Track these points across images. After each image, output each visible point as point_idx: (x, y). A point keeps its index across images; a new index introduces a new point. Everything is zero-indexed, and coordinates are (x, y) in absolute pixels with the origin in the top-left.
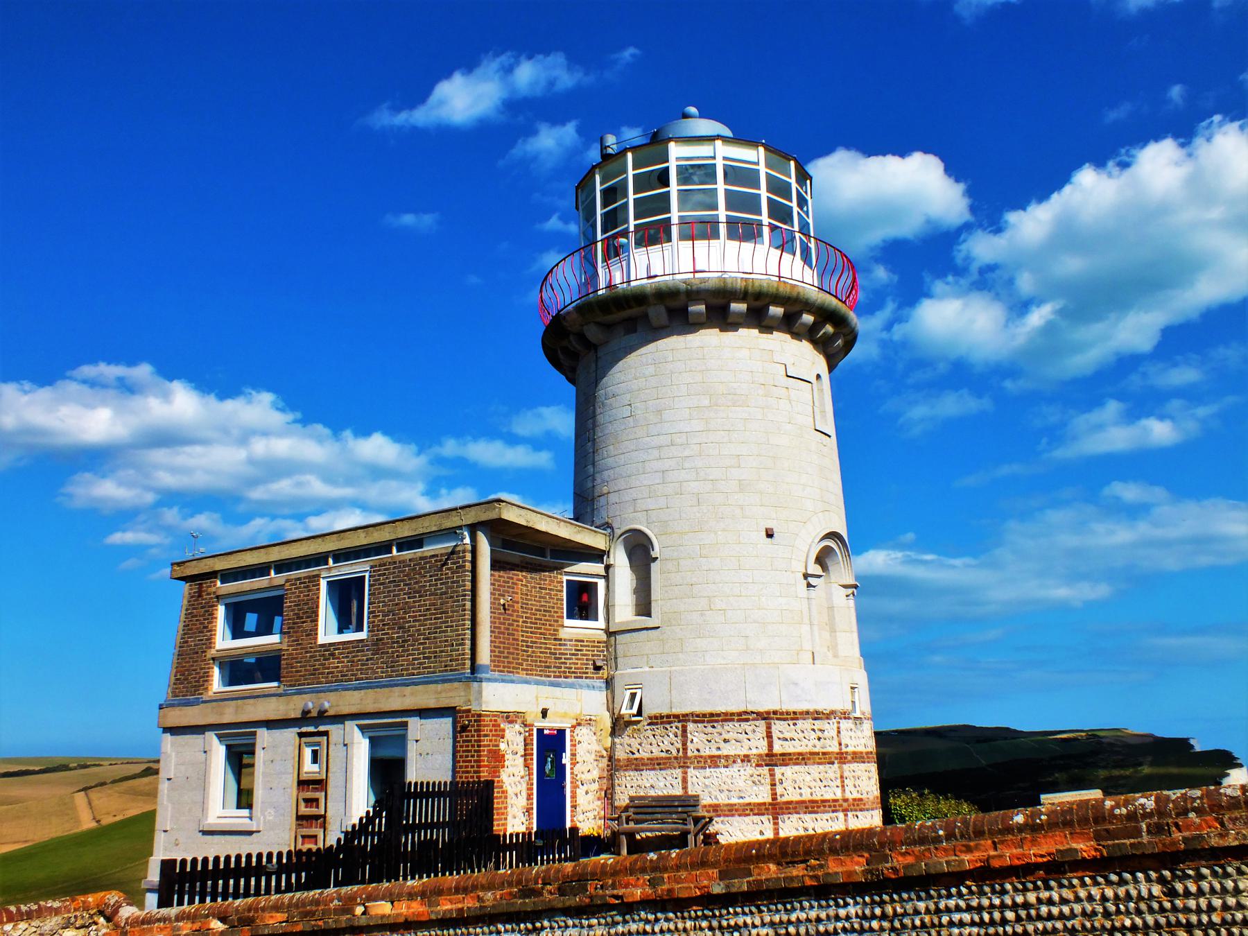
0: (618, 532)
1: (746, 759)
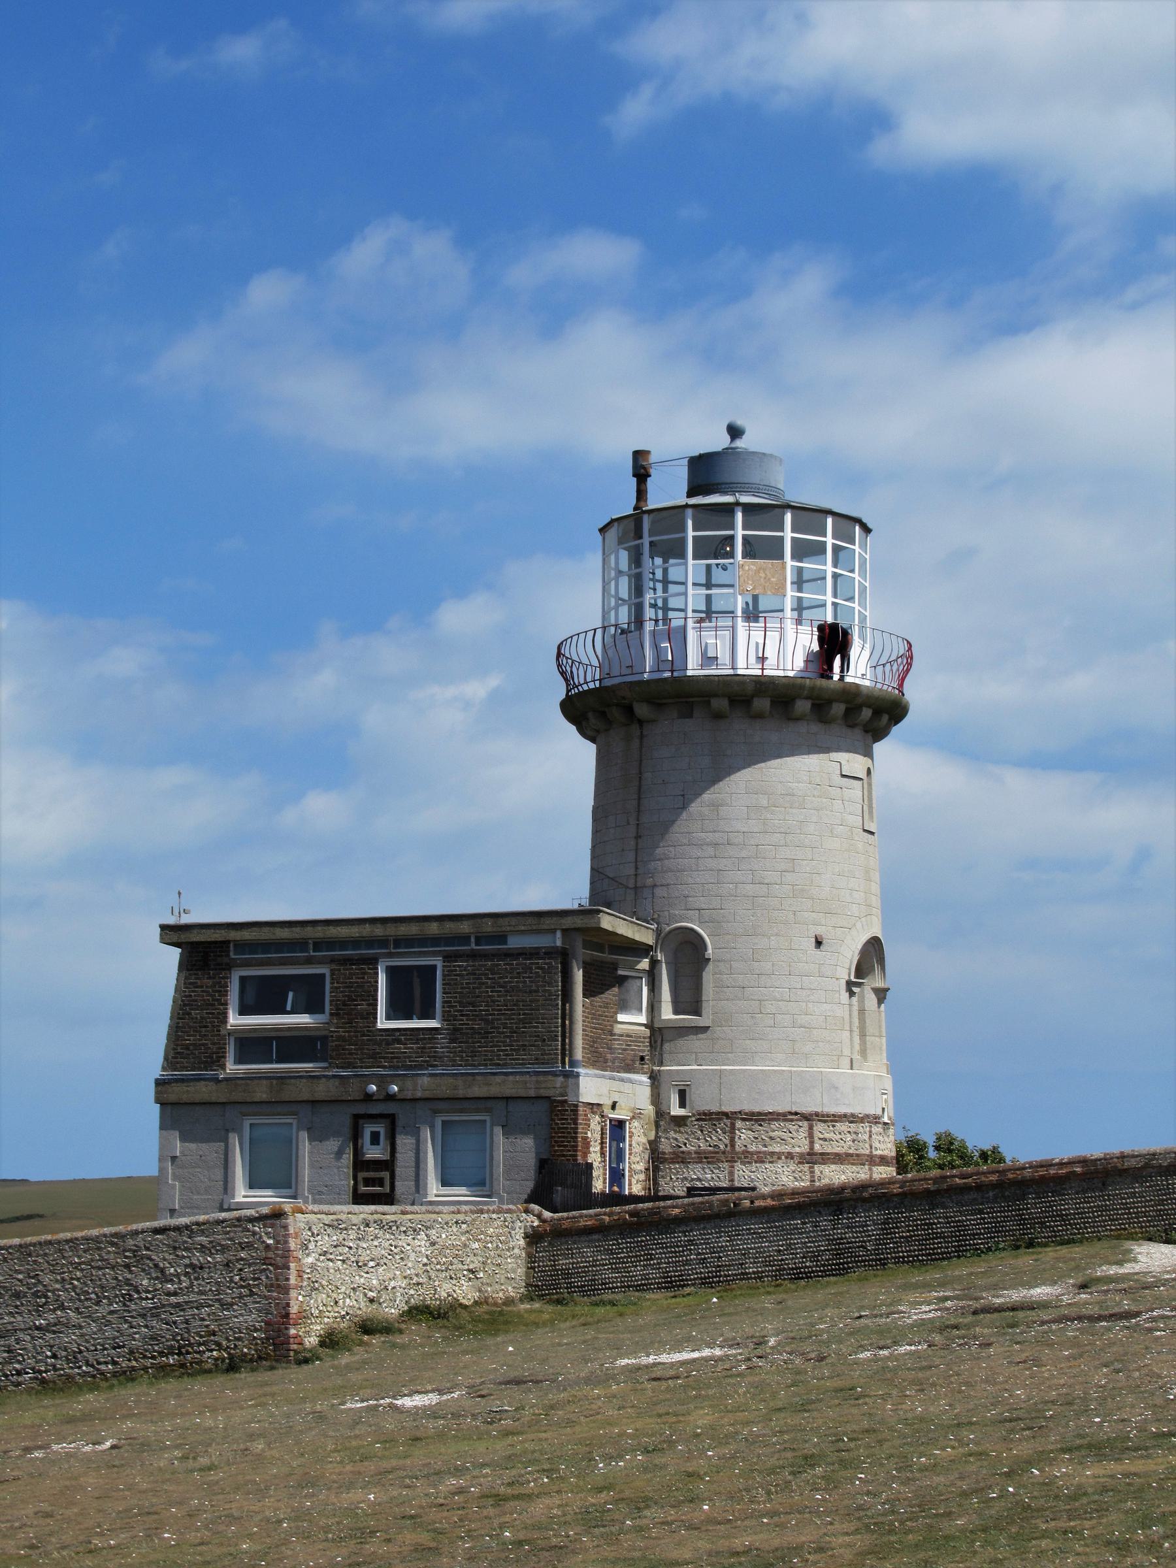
1: (790, 1156)
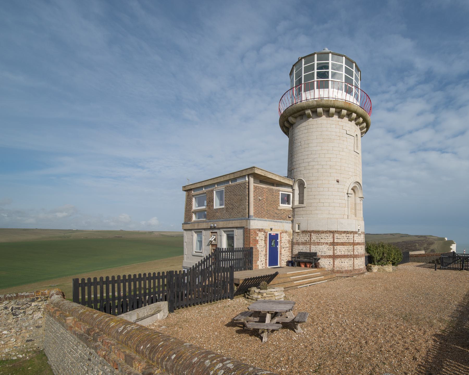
0: (296, 180)
1: (327, 243)
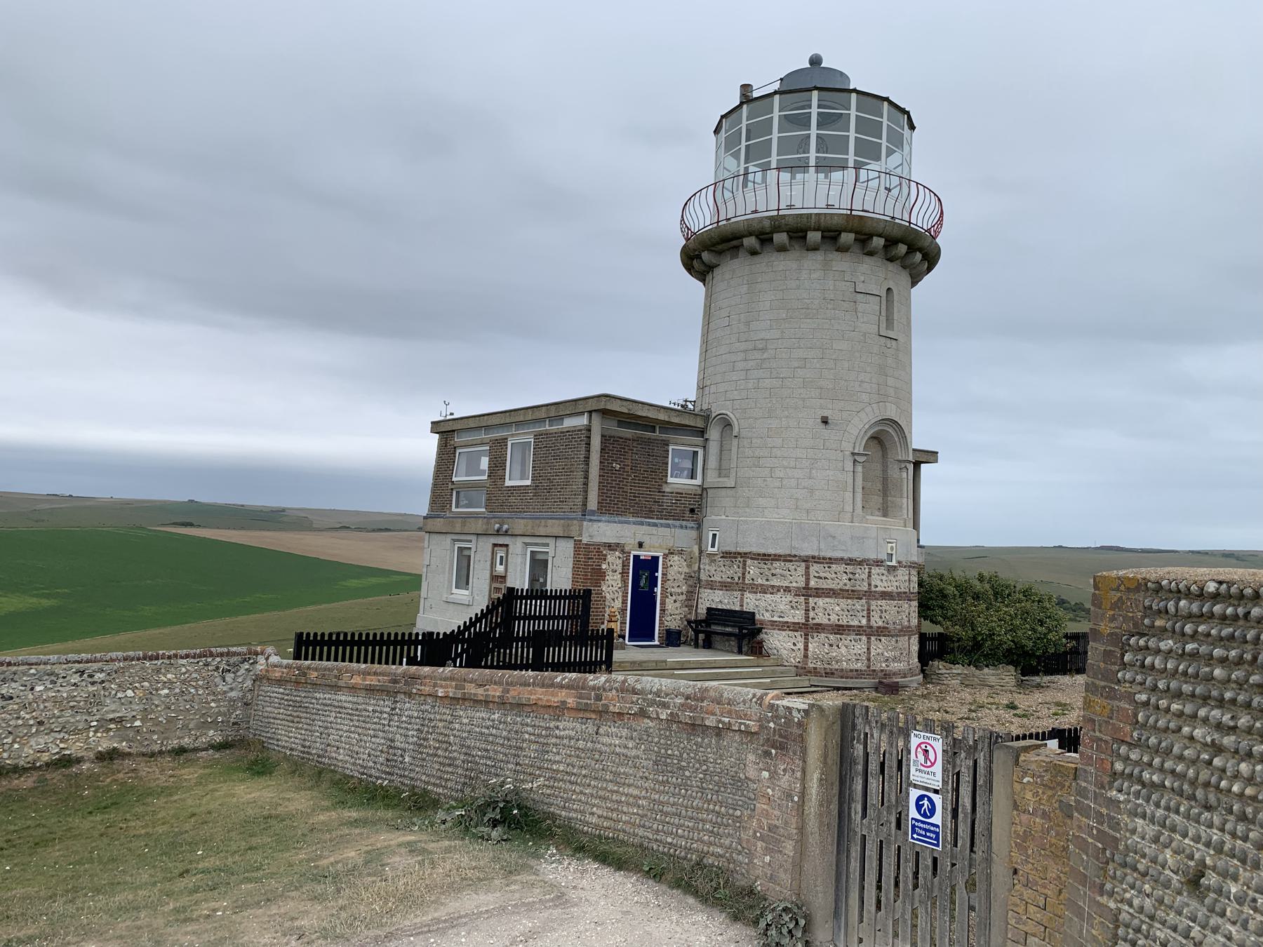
1: (787, 590)
